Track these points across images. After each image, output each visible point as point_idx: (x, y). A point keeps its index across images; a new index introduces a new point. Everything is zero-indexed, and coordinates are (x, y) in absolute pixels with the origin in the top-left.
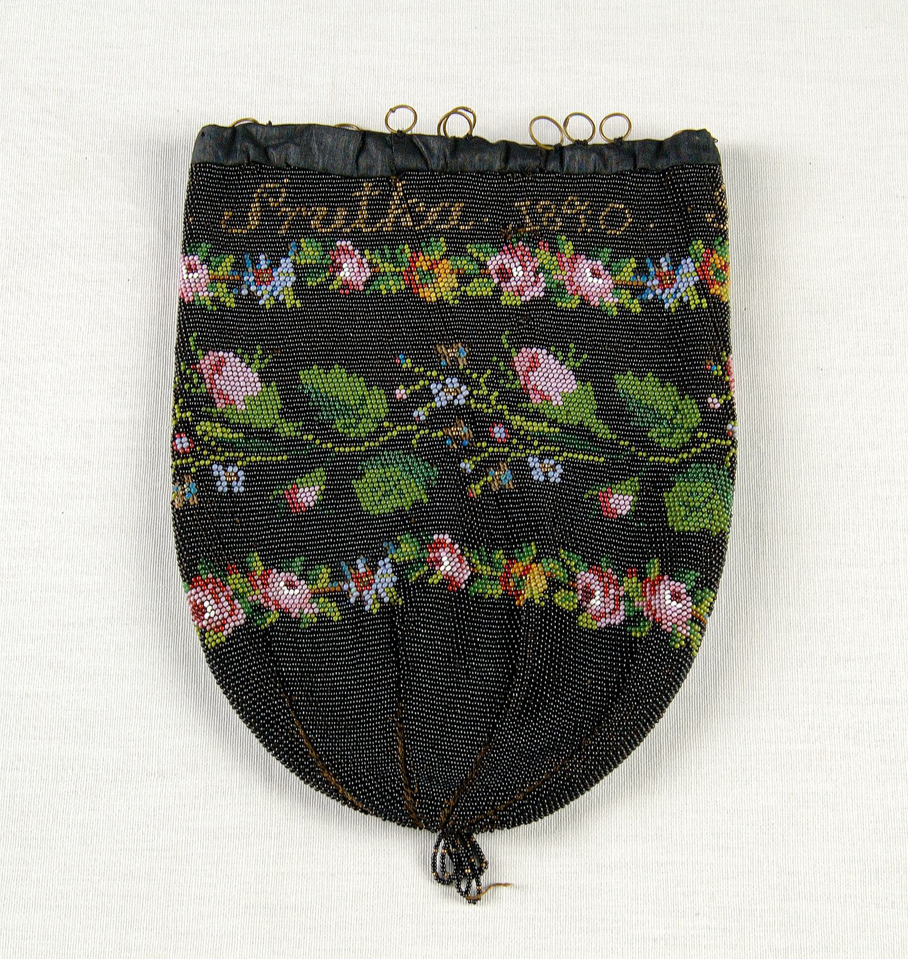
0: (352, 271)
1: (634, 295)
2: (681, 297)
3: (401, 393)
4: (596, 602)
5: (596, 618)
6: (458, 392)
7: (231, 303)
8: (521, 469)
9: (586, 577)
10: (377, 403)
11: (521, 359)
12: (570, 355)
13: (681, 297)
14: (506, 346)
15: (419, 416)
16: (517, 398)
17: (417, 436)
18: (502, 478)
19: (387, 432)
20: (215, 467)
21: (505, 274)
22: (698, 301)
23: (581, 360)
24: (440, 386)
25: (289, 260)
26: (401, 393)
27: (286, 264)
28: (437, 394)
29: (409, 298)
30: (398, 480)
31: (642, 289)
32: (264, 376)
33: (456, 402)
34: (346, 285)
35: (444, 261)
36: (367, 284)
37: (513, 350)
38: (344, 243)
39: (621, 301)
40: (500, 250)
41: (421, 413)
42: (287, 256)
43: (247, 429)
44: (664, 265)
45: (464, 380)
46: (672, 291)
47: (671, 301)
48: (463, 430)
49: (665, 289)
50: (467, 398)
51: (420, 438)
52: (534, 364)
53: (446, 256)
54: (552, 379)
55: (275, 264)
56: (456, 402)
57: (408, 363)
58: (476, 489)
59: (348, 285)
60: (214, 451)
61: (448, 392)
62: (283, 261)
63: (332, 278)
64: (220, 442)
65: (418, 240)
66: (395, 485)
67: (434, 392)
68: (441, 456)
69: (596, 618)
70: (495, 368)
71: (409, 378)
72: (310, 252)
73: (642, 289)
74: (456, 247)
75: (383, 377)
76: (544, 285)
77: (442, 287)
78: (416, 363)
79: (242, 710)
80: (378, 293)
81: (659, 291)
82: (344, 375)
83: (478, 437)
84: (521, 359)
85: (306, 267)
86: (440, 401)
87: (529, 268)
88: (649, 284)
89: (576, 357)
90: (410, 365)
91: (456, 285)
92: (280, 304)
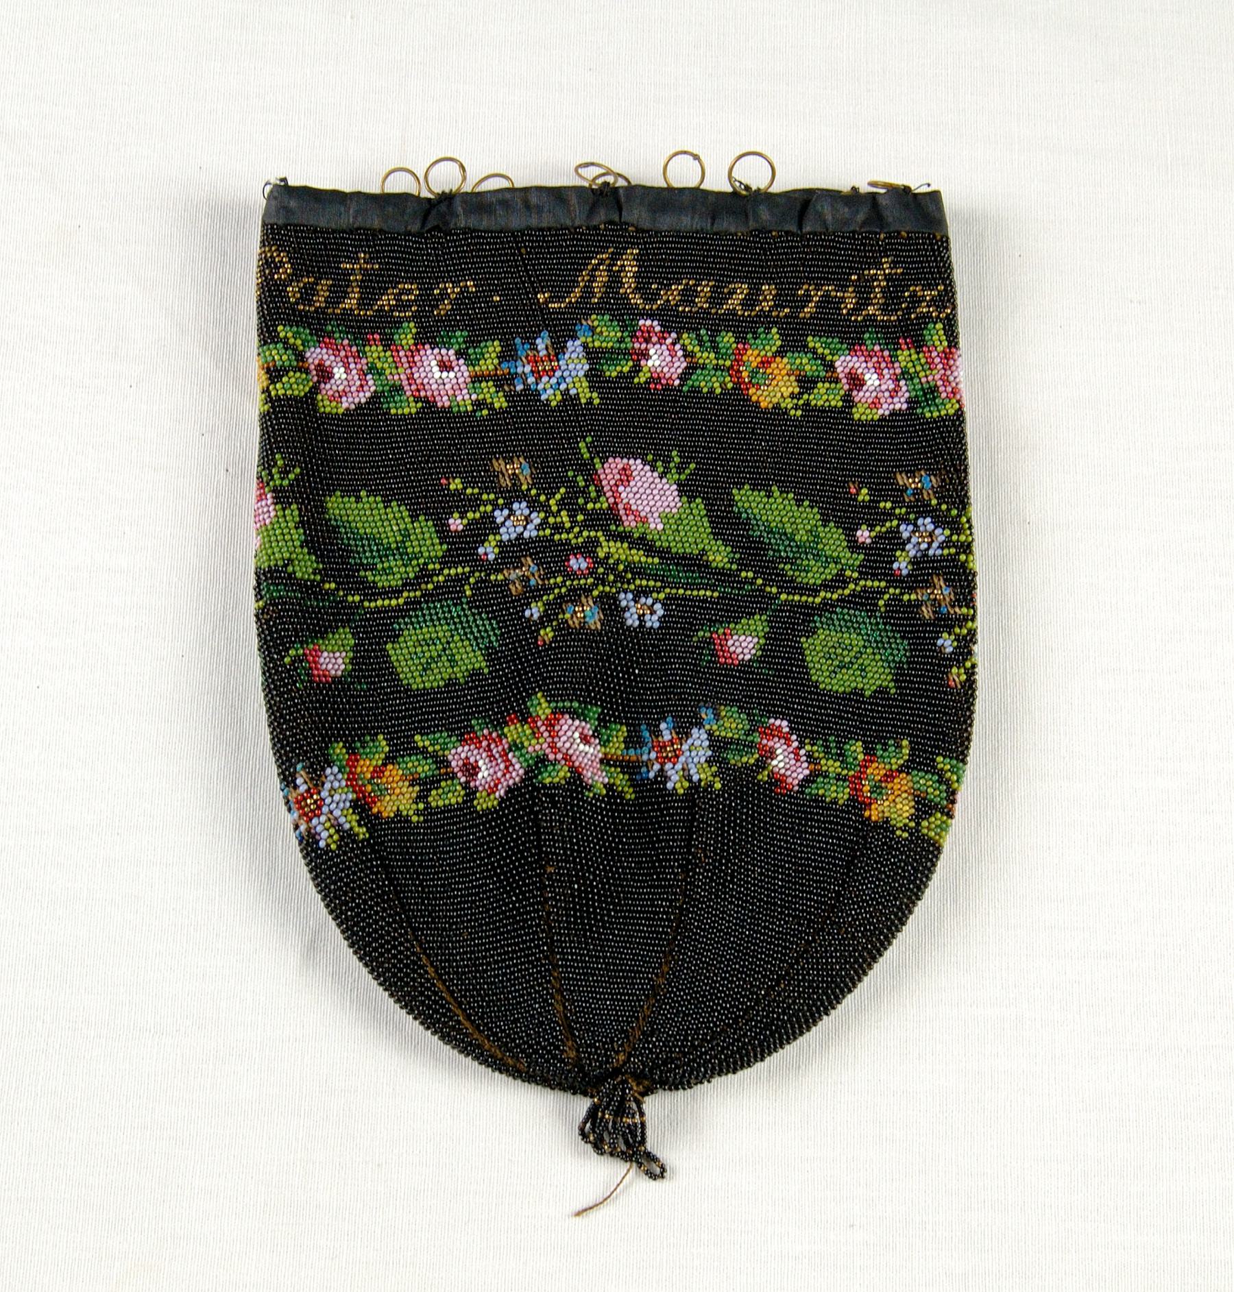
0: (661, 361)
1: (499, 387)
2: (568, 389)
3: (456, 523)
4: (484, 774)
5: (491, 791)
6: (528, 520)
7: (500, 402)
8: (610, 607)
9: (458, 754)
10: (426, 542)
11: (610, 470)
12: (672, 465)
13: (568, 389)
14: (587, 456)
15: (486, 554)
16: (607, 521)
17: (472, 580)
18: (589, 614)
19: (431, 576)
20: (622, 596)
21: (856, 381)
22: (588, 395)
23: (688, 471)
24: (506, 512)
25: (578, 343)
26: (456, 523)
27: (574, 348)
28: (503, 524)
29: (737, 400)
30: (448, 643)
31: (510, 378)
32: (684, 489)
33: (526, 535)
34: (655, 379)
35: (778, 359)
36: (684, 377)
37: (596, 460)
38: (649, 323)
39: (481, 397)
40: (851, 350)
41: (489, 550)
42: (574, 338)
43: (664, 553)
44: (541, 346)
45: (533, 505)
46: (554, 380)
47: (550, 392)
48: (530, 567)
49: (541, 377)
50: (540, 527)
51: (477, 582)
52: (626, 476)
53: (781, 353)
54: (649, 495)
55: (558, 349)
56: (526, 535)
57: (456, 484)
58: (547, 634)
59: (659, 378)
60: (622, 577)
61: (518, 523)
62: (569, 344)
63: (637, 369)
64: (630, 567)
65: (745, 329)
66: (444, 650)
67: (499, 520)
68: (497, 603)
69: (491, 791)
70: (571, 484)
71: (463, 504)
72: (607, 333)
73: (510, 378)
74: (793, 343)
75: (434, 506)
76: (907, 395)
77: (776, 390)
78: (467, 483)
79: (348, 929)
80: (696, 391)
81: (531, 380)
82: (381, 505)
83: (551, 574)
84: (610, 470)
85: (603, 351)
86: (508, 533)
87: (887, 377)
88: (520, 370)
89: (680, 469)
90: (460, 486)
91: (797, 390)
92: (569, 400)
